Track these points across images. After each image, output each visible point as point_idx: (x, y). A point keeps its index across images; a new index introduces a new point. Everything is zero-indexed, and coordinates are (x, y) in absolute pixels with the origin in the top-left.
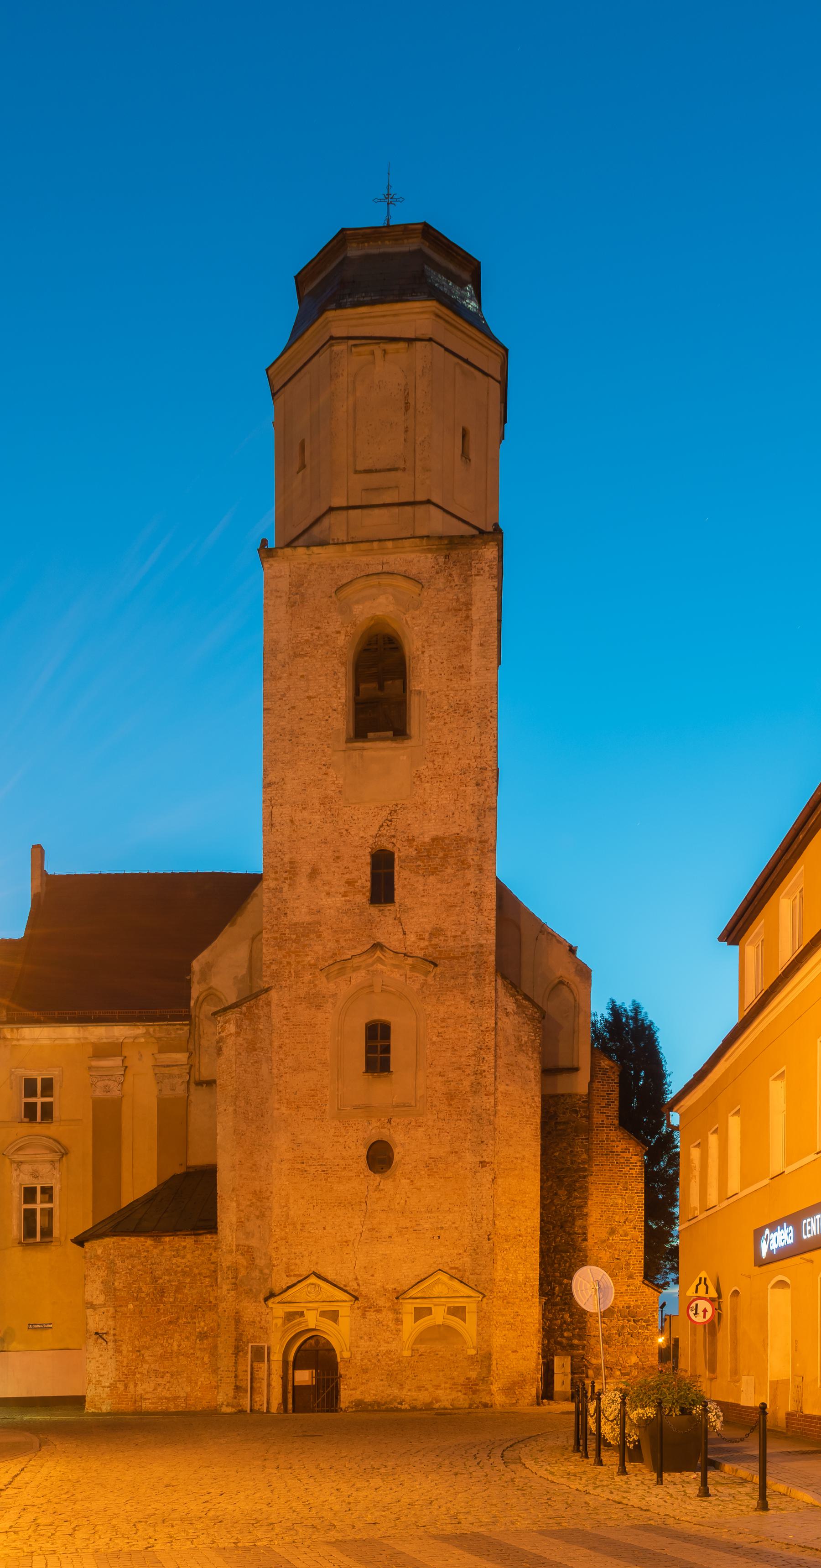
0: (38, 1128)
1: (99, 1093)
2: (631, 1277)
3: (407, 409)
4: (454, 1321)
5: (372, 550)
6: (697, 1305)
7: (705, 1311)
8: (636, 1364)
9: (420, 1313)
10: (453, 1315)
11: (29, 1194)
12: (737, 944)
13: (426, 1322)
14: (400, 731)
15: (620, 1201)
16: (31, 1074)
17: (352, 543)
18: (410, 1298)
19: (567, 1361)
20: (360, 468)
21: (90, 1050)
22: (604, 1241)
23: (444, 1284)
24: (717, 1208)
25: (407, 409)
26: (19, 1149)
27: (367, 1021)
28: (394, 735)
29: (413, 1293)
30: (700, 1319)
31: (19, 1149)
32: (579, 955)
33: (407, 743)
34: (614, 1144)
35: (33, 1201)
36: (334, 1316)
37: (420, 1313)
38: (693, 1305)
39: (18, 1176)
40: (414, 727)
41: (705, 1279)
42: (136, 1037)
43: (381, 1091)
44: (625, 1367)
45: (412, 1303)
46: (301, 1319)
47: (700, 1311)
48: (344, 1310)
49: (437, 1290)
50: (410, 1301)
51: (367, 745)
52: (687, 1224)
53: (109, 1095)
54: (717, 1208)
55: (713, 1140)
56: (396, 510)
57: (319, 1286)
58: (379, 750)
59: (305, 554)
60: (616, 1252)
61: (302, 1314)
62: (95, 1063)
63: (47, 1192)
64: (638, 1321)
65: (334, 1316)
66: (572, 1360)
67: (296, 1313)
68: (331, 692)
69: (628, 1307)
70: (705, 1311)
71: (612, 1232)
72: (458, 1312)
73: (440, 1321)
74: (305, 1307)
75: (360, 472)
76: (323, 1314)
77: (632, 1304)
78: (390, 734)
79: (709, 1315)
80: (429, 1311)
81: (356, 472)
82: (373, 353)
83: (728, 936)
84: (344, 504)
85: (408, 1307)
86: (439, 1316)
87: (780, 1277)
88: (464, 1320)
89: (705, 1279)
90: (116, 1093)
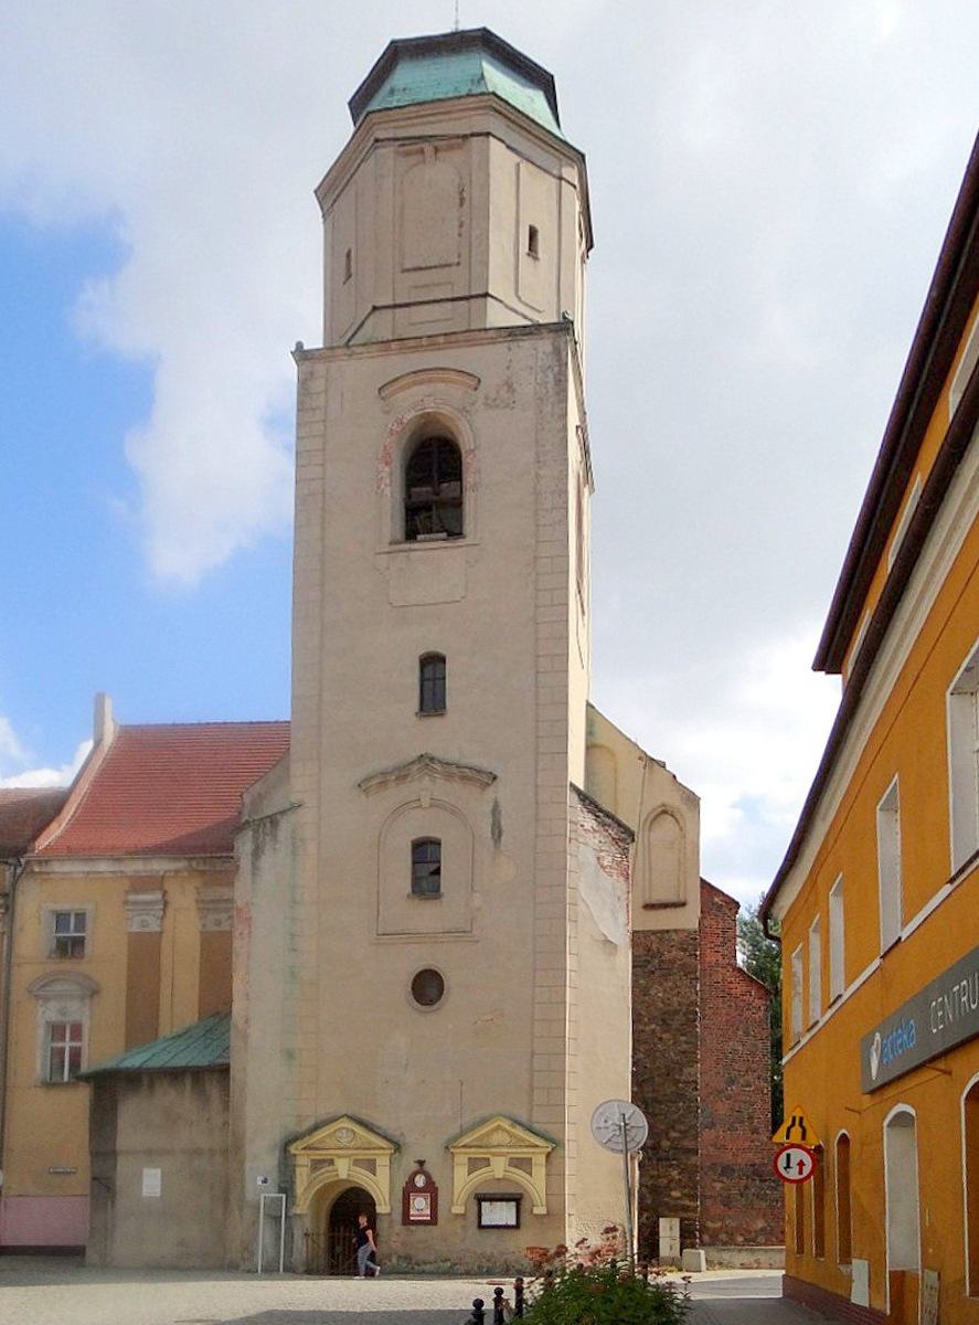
0: (67, 965)
1: (135, 928)
2: (755, 1131)
3: (461, 204)
4: (518, 1175)
5: (422, 346)
6: (788, 1156)
7: (801, 1164)
8: (762, 1229)
9: (474, 1165)
10: (516, 1167)
11: (56, 1031)
12: (840, 673)
13: (481, 1174)
14: (455, 533)
15: (740, 1048)
16: (60, 907)
17: (398, 340)
18: (464, 1146)
19: (676, 1222)
20: (408, 266)
21: (126, 885)
22: (722, 1091)
23: (505, 1130)
24: (821, 1024)
25: (461, 204)
26: (43, 986)
27: (414, 837)
28: (449, 535)
29: (466, 1140)
30: (793, 1174)
31: (43, 986)
32: (668, 768)
33: (460, 542)
34: (732, 986)
35: (63, 1038)
36: (371, 1166)
37: (474, 1165)
38: (784, 1155)
39: (43, 1012)
40: (468, 527)
41: (801, 1119)
42: (177, 871)
43: (427, 916)
44: (750, 1232)
45: (465, 1153)
46: (331, 1168)
47: (794, 1163)
48: (383, 1162)
49: (497, 1138)
50: (463, 1150)
51: (415, 546)
52: (791, 1054)
53: (147, 930)
54: (821, 1024)
55: (815, 940)
56: (449, 305)
57: (354, 1133)
58: (432, 553)
59: (345, 355)
60: (737, 1105)
61: (331, 1162)
62: (131, 897)
63: (77, 1032)
64: (766, 1180)
65: (371, 1166)
66: (681, 1223)
67: (324, 1161)
68: (380, 493)
69: (753, 1165)
70: (801, 1164)
71: (732, 1082)
72: (523, 1164)
73: (499, 1174)
74: (336, 1155)
75: (408, 270)
76: (357, 1163)
77: (757, 1161)
78: (444, 535)
79: (807, 1170)
80: (487, 1162)
81: (404, 271)
82: (422, 151)
83: (824, 665)
84: (391, 303)
85: (461, 1159)
86: (499, 1167)
87: (901, 1107)
88: (531, 1175)
89: (801, 1119)
90: (155, 928)
